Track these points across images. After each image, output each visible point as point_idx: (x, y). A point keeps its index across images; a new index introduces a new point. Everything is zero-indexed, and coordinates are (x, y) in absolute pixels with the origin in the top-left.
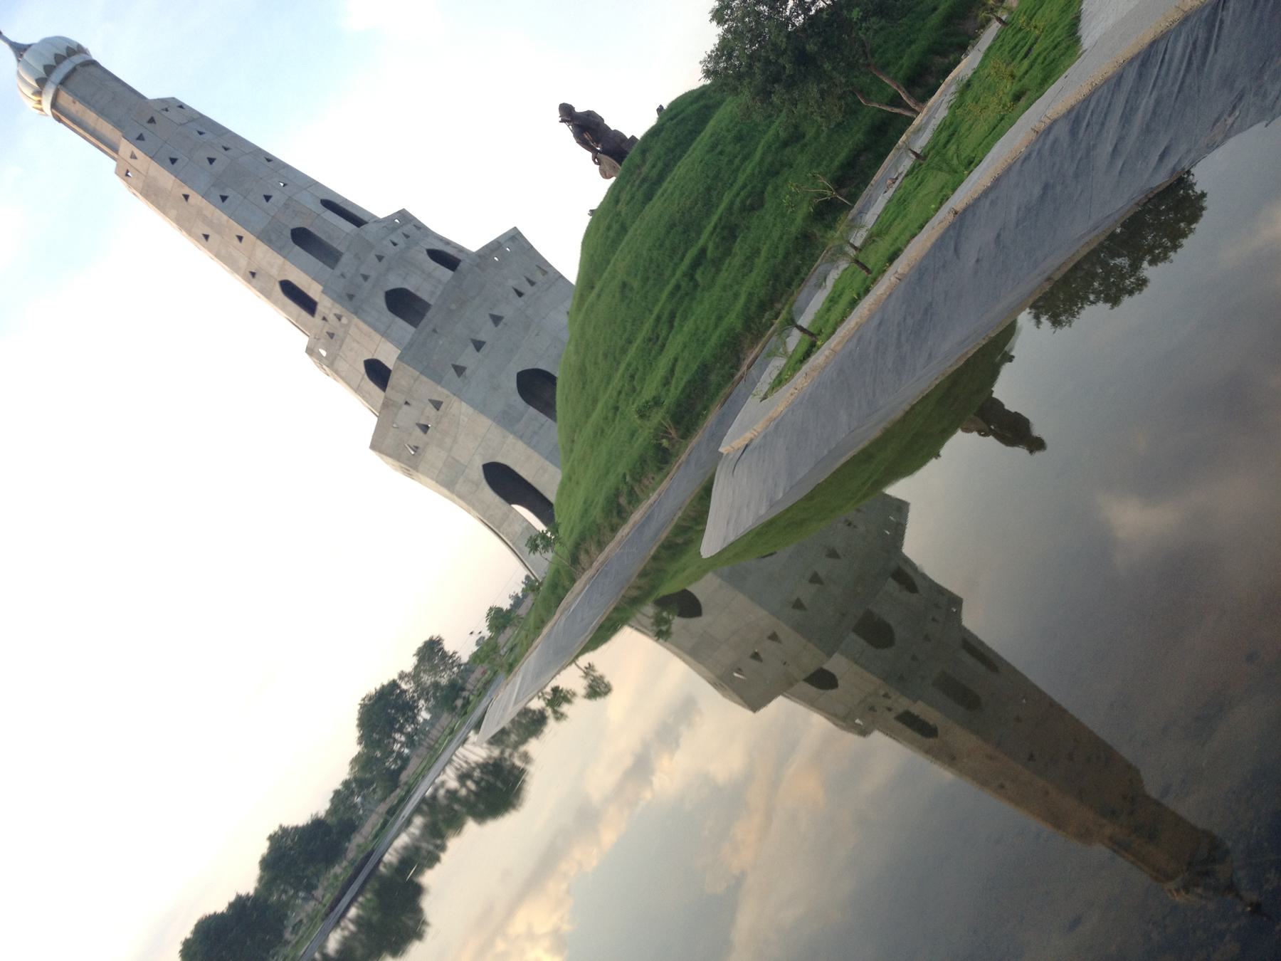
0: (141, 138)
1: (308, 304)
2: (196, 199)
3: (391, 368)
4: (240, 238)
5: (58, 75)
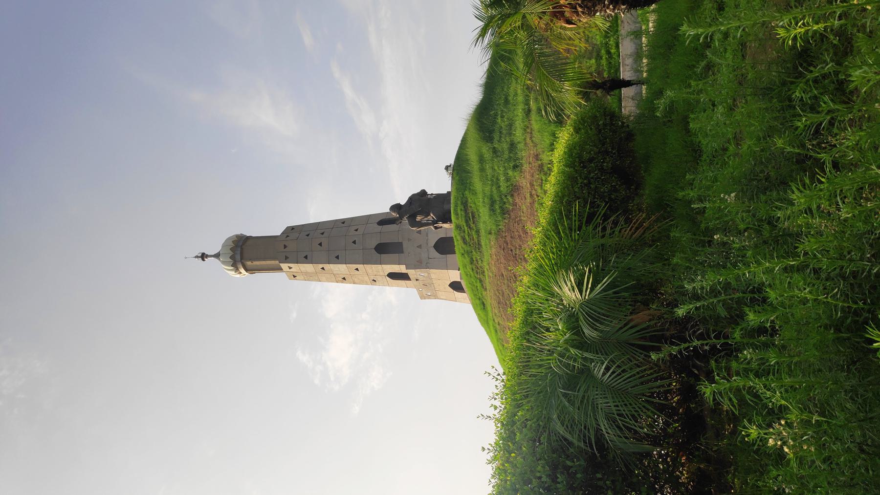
0: (286, 258)
1: (404, 277)
2: (326, 266)
3: (459, 280)
4: (357, 269)
5: (238, 257)
